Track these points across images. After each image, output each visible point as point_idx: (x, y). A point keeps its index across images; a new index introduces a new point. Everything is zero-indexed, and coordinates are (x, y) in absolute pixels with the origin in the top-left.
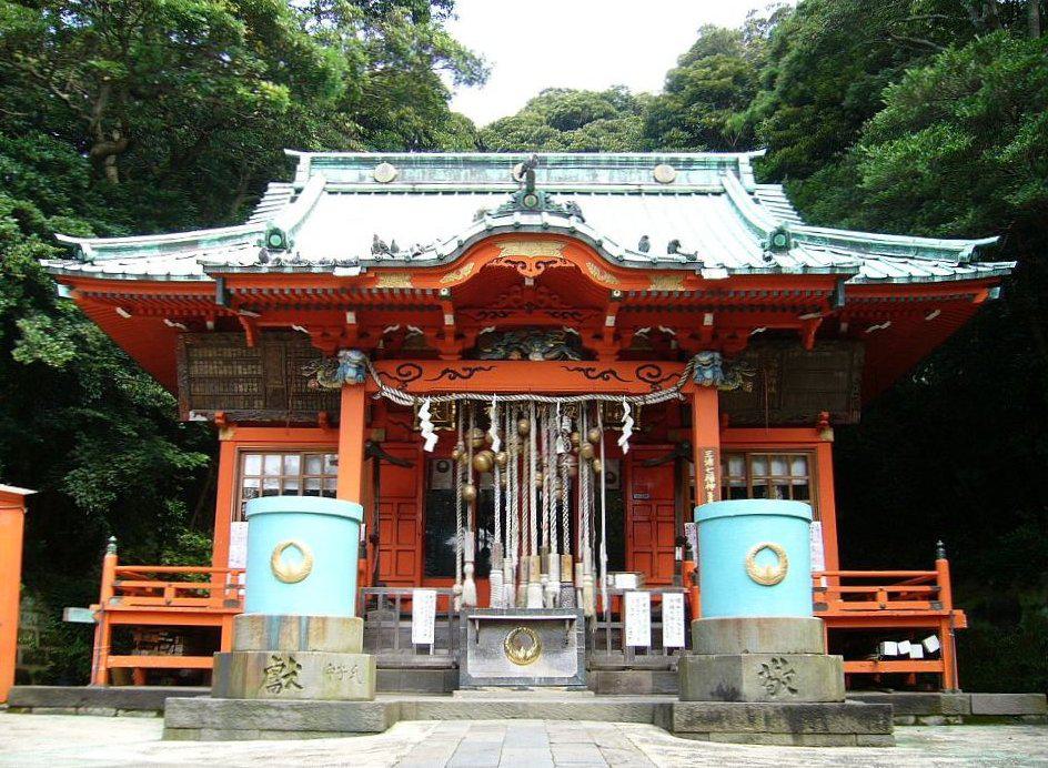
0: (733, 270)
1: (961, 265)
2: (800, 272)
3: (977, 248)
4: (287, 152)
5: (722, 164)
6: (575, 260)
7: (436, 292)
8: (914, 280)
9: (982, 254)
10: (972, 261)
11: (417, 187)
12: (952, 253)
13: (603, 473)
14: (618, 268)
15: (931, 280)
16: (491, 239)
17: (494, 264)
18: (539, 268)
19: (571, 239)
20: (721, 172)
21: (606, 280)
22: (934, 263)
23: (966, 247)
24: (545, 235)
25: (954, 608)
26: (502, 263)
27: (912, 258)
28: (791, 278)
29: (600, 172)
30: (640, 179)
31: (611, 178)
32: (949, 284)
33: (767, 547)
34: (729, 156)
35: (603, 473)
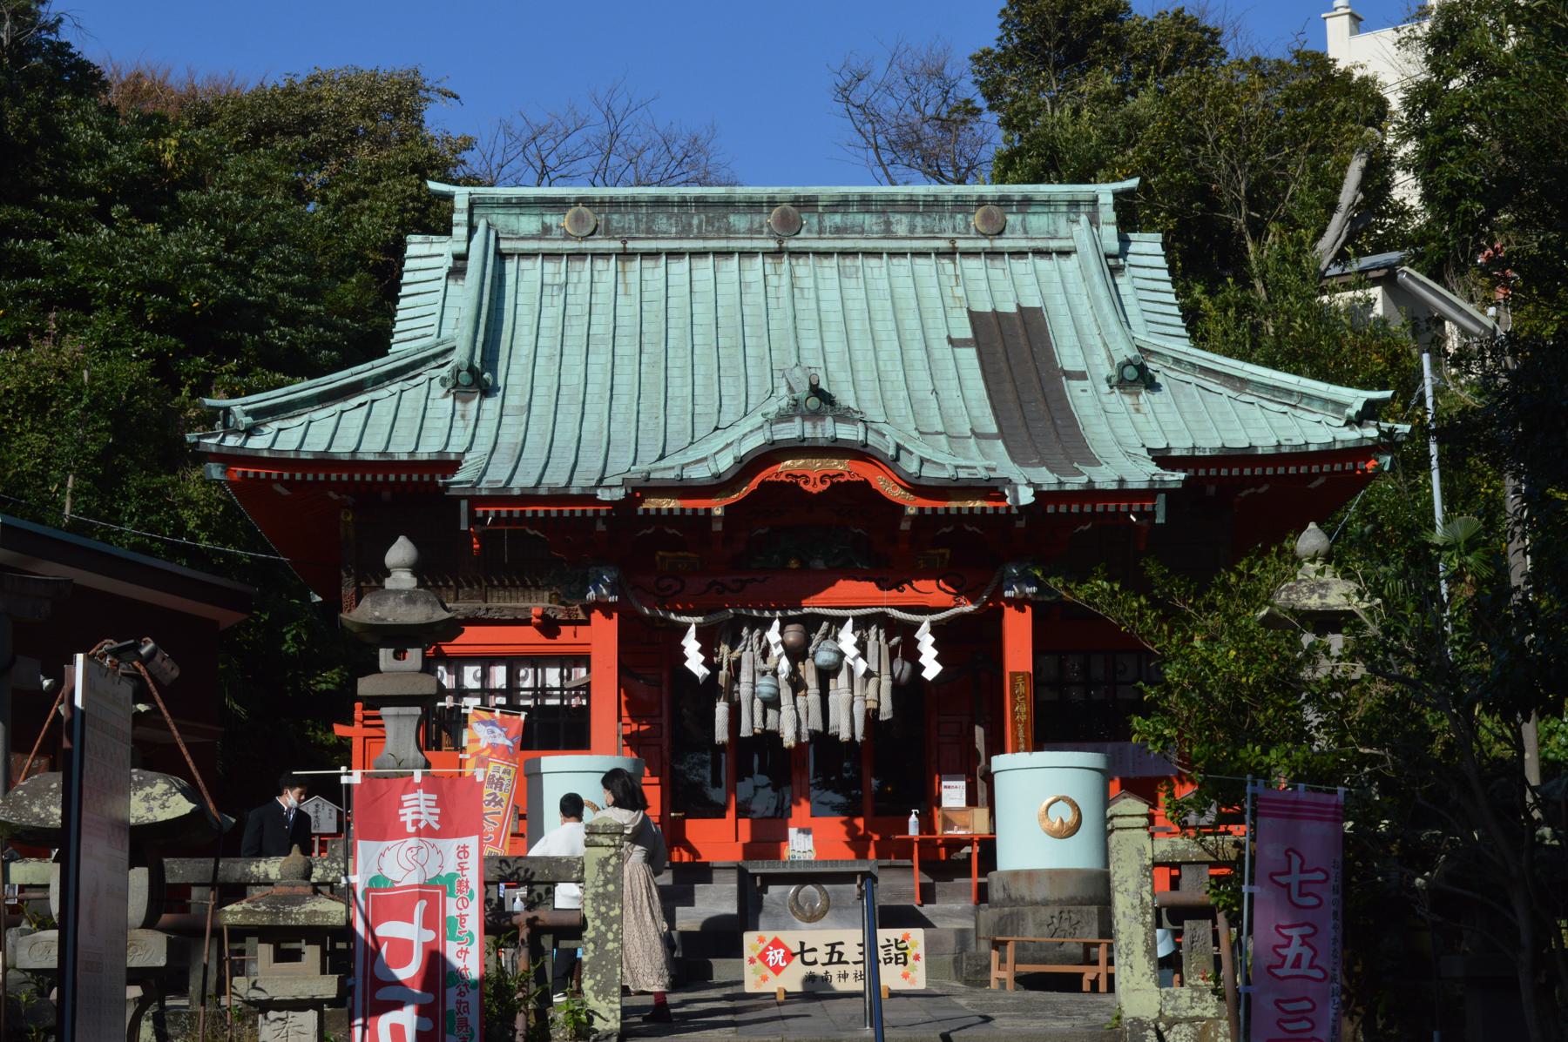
0: (1040, 485)
1: (1349, 423)
2: (1114, 486)
3: (1369, 404)
4: (433, 185)
5: (1074, 204)
6: (862, 471)
7: (708, 511)
8: (1284, 450)
9: (1371, 412)
10: (1358, 421)
11: (631, 245)
12: (1339, 406)
13: (1118, 186)
14: (918, 488)
15: (1304, 449)
16: (772, 454)
17: (773, 478)
18: (822, 481)
19: (860, 452)
20: (1072, 216)
21: (895, 493)
22: (1318, 417)
23: (1355, 398)
24: (837, 449)
25: (580, 819)
26: (783, 477)
27: (1295, 407)
28: (1105, 495)
29: (894, 218)
30: (954, 229)
31: (912, 229)
32: (1328, 454)
33: (1080, 815)
34: (1082, 190)
35: (1118, 186)
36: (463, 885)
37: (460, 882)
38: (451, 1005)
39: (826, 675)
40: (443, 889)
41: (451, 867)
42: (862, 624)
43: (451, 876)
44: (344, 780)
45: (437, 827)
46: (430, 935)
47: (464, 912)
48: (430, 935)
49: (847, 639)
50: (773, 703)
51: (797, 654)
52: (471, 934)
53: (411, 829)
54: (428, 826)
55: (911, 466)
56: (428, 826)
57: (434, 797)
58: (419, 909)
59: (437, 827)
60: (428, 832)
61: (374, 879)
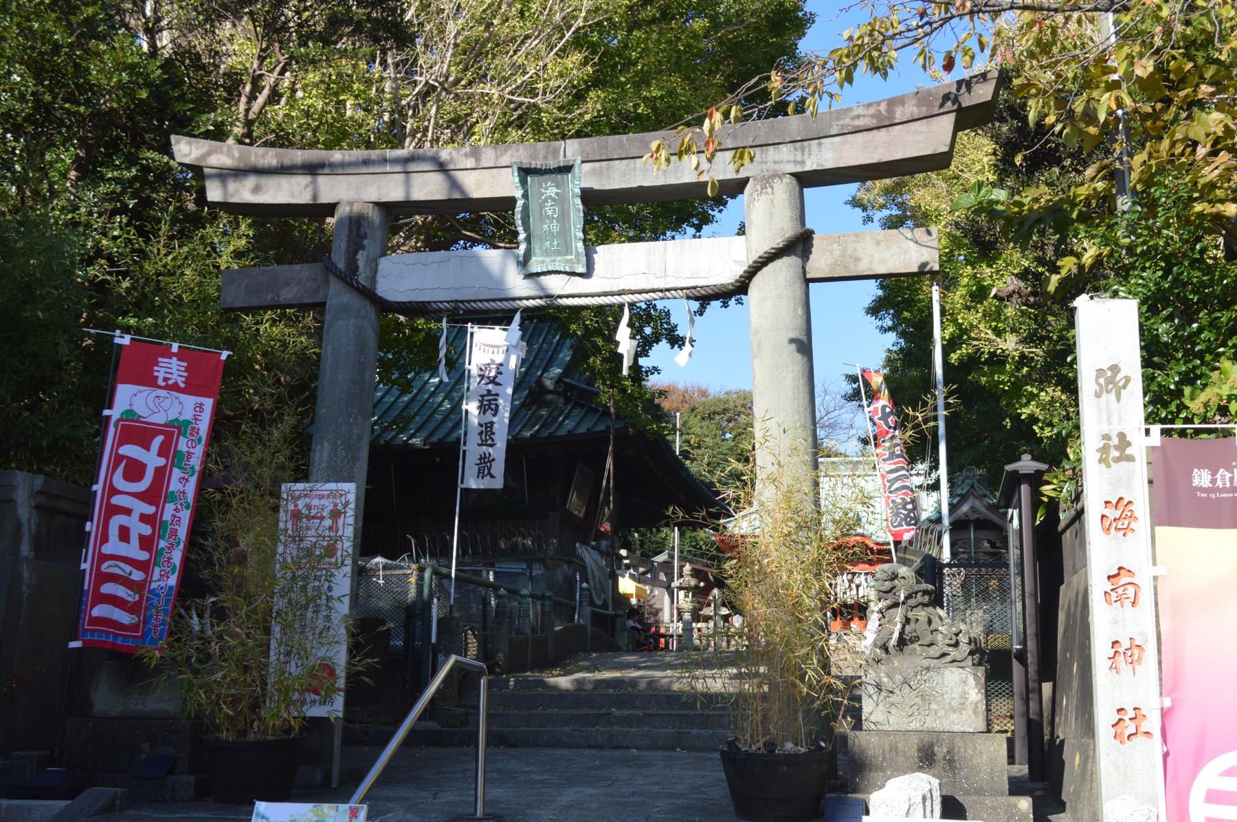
14: (877, 544)
19: (863, 535)
36: (195, 431)
37: (193, 428)
38: (167, 517)
39: (858, 586)
40: (179, 429)
41: (188, 415)
42: (866, 574)
43: (187, 422)
44: (117, 341)
45: (182, 385)
46: (161, 462)
47: (191, 450)
48: (161, 462)
49: (863, 577)
50: (845, 593)
51: (851, 581)
52: (193, 468)
53: (161, 382)
54: (176, 384)
55: (874, 538)
56: (176, 384)
57: (185, 364)
58: (159, 440)
59: (182, 385)
60: (175, 387)
61: (126, 412)
